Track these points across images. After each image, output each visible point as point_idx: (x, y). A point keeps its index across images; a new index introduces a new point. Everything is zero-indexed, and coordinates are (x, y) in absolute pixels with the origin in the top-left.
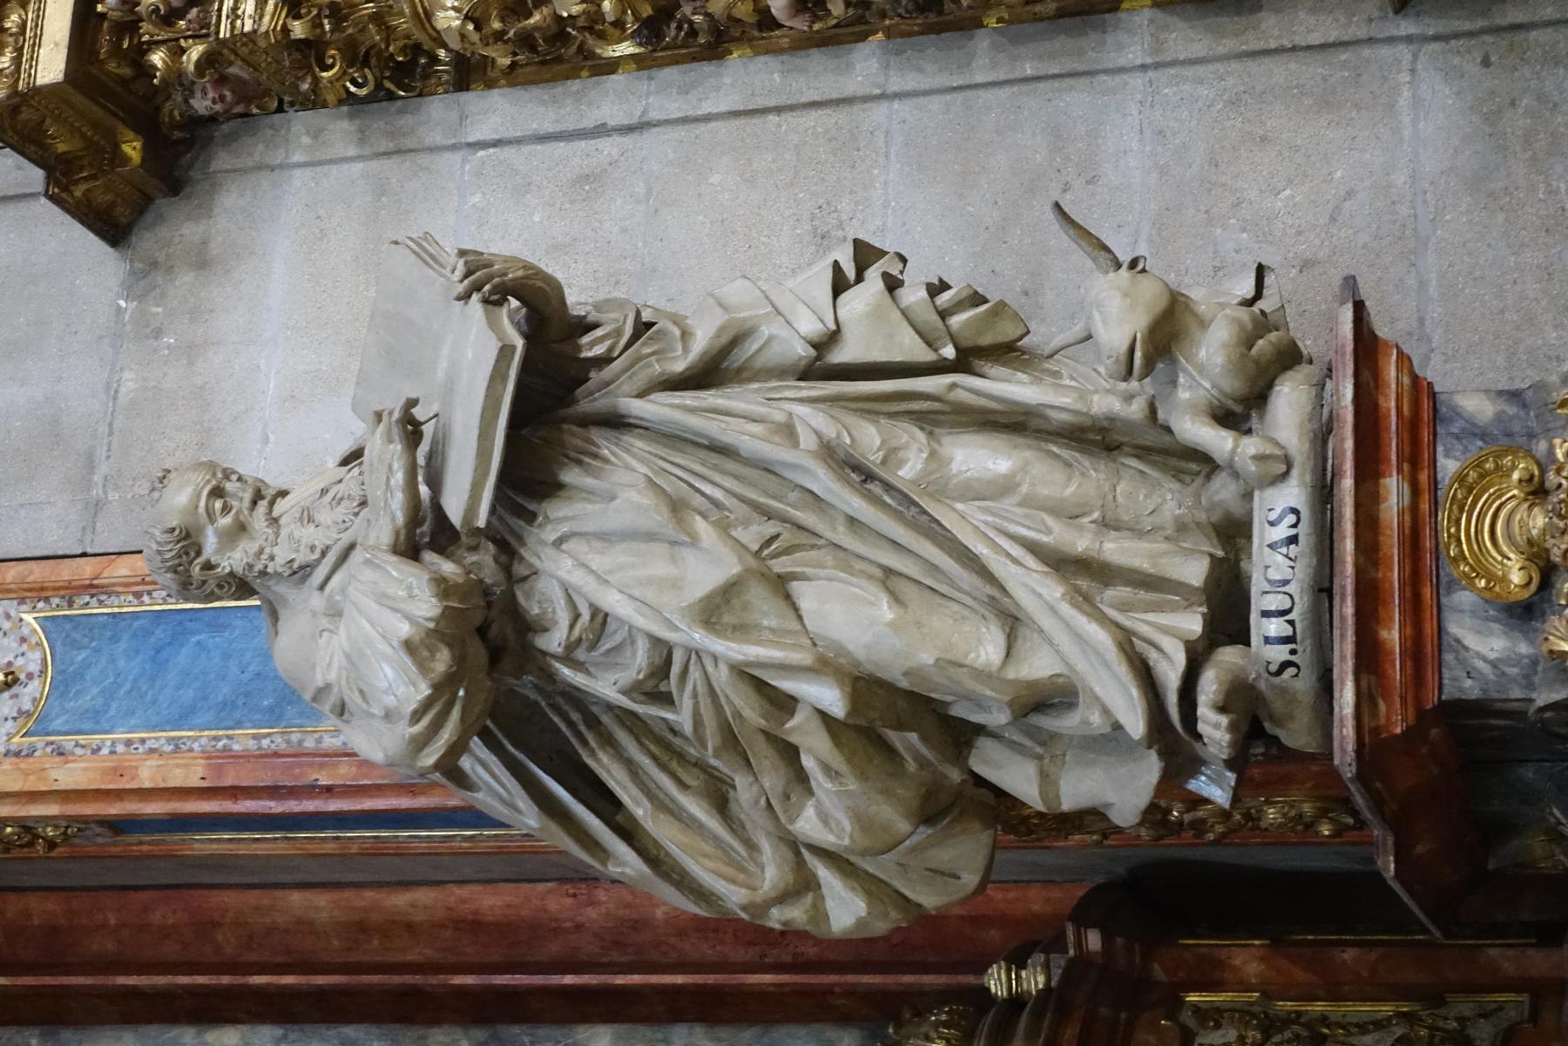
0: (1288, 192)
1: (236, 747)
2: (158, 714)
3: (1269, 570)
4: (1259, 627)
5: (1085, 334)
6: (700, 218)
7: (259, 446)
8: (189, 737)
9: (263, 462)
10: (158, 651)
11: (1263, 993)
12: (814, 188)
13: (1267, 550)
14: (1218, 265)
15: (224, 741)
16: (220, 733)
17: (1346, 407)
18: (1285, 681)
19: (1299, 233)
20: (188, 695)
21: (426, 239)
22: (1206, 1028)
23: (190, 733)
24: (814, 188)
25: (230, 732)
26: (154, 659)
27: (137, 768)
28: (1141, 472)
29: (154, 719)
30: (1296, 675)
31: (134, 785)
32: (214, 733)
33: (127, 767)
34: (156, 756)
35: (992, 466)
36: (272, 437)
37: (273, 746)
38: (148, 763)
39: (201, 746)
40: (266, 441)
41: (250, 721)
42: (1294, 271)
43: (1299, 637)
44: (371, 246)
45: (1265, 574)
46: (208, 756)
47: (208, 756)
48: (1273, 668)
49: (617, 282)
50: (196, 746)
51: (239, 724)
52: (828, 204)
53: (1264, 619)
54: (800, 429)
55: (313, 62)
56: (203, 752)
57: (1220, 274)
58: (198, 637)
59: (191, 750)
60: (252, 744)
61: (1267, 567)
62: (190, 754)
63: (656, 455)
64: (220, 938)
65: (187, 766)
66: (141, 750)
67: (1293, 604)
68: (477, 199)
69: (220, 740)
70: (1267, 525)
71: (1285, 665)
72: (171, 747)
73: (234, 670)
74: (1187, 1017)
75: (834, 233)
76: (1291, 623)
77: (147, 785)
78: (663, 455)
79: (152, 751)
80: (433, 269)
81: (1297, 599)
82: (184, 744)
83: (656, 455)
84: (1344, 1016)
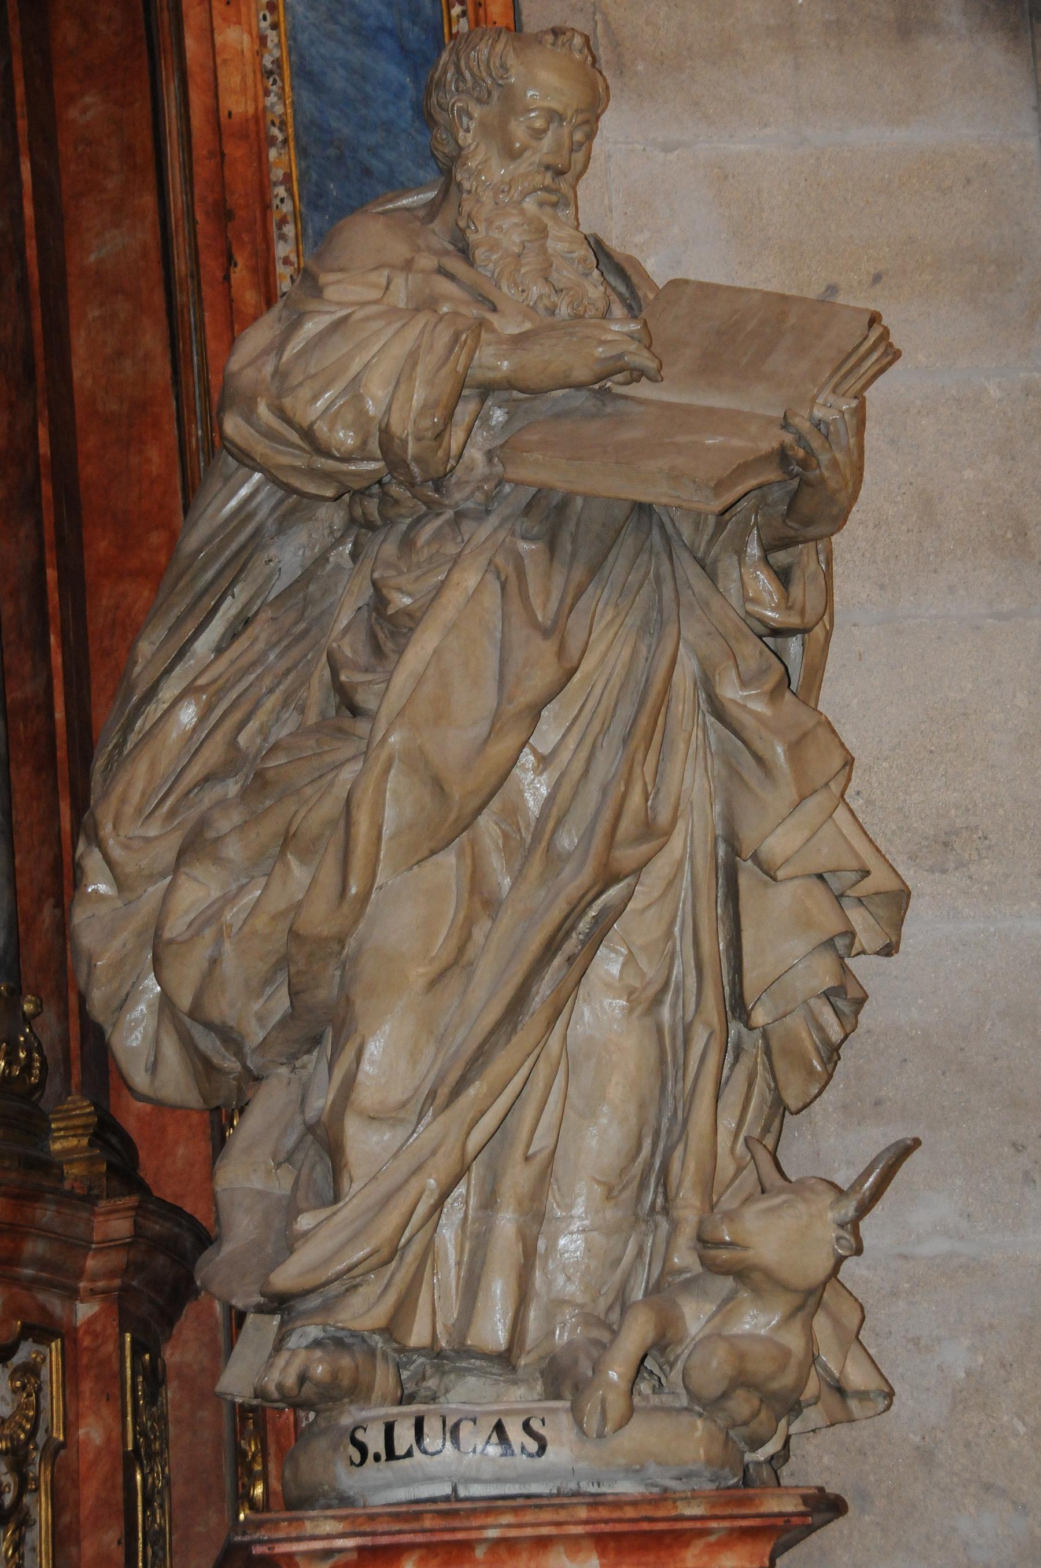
0: (1021, 1429)
1: (273, 153)
2: (312, 43)
3: (472, 1423)
4: (405, 1415)
5: (767, 1185)
6: (970, 686)
7: (660, 140)
8: (283, 88)
9: (640, 147)
10: (391, 33)
11: (63, 1445)
12: (1011, 827)
13: (494, 1421)
14: (923, 1343)
15: (280, 137)
16: (291, 131)
17: (676, 1507)
18: (345, 1449)
19: (967, 1445)
20: (337, 80)
21: (885, 353)
22: (12, 1378)
23: (287, 89)
24: (1011, 827)
25: (292, 144)
26: (382, 29)
27: (239, 23)
28: (619, 1260)
29: (303, 38)
30: (352, 1463)
31: (217, 21)
32: (290, 121)
33: (239, 10)
34: (256, 47)
35: (614, 1080)
36: (672, 156)
37: (277, 201)
38: (246, 38)
39: (273, 105)
40: (667, 148)
41: (308, 167)
42: (918, 1439)
43: (394, 1463)
44: (929, 258)
45: (466, 1419)
46: (259, 117)
47: (259, 117)
48: (360, 1435)
49: (882, 587)
50: (272, 99)
51: (302, 152)
52: (990, 847)
53: (413, 1421)
54: (645, 848)
55: (329, 567)
56: (265, 108)
57: (910, 1346)
58: (411, 86)
59: (267, 93)
60: (278, 174)
61: (474, 1421)
62: (261, 93)
63: (611, 674)
64: (88, 99)
65: (244, 91)
66: (264, 25)
67: (433, 1454)
68: (994, 392)
69: (281, 130)
70: (524, 1418)
71: (362, 1448)
72: (269, 66)
73: (371, 139)
74: (26, 1352)
75: (951, 857)
76: (409, 1454)
77: (219, 39)
78: (612, 683)
79: (263, 40)
80: (832, 376)
81: (436, 1458)
82: (275, 82)
83: (611, 674)
84: (34, 1549)
